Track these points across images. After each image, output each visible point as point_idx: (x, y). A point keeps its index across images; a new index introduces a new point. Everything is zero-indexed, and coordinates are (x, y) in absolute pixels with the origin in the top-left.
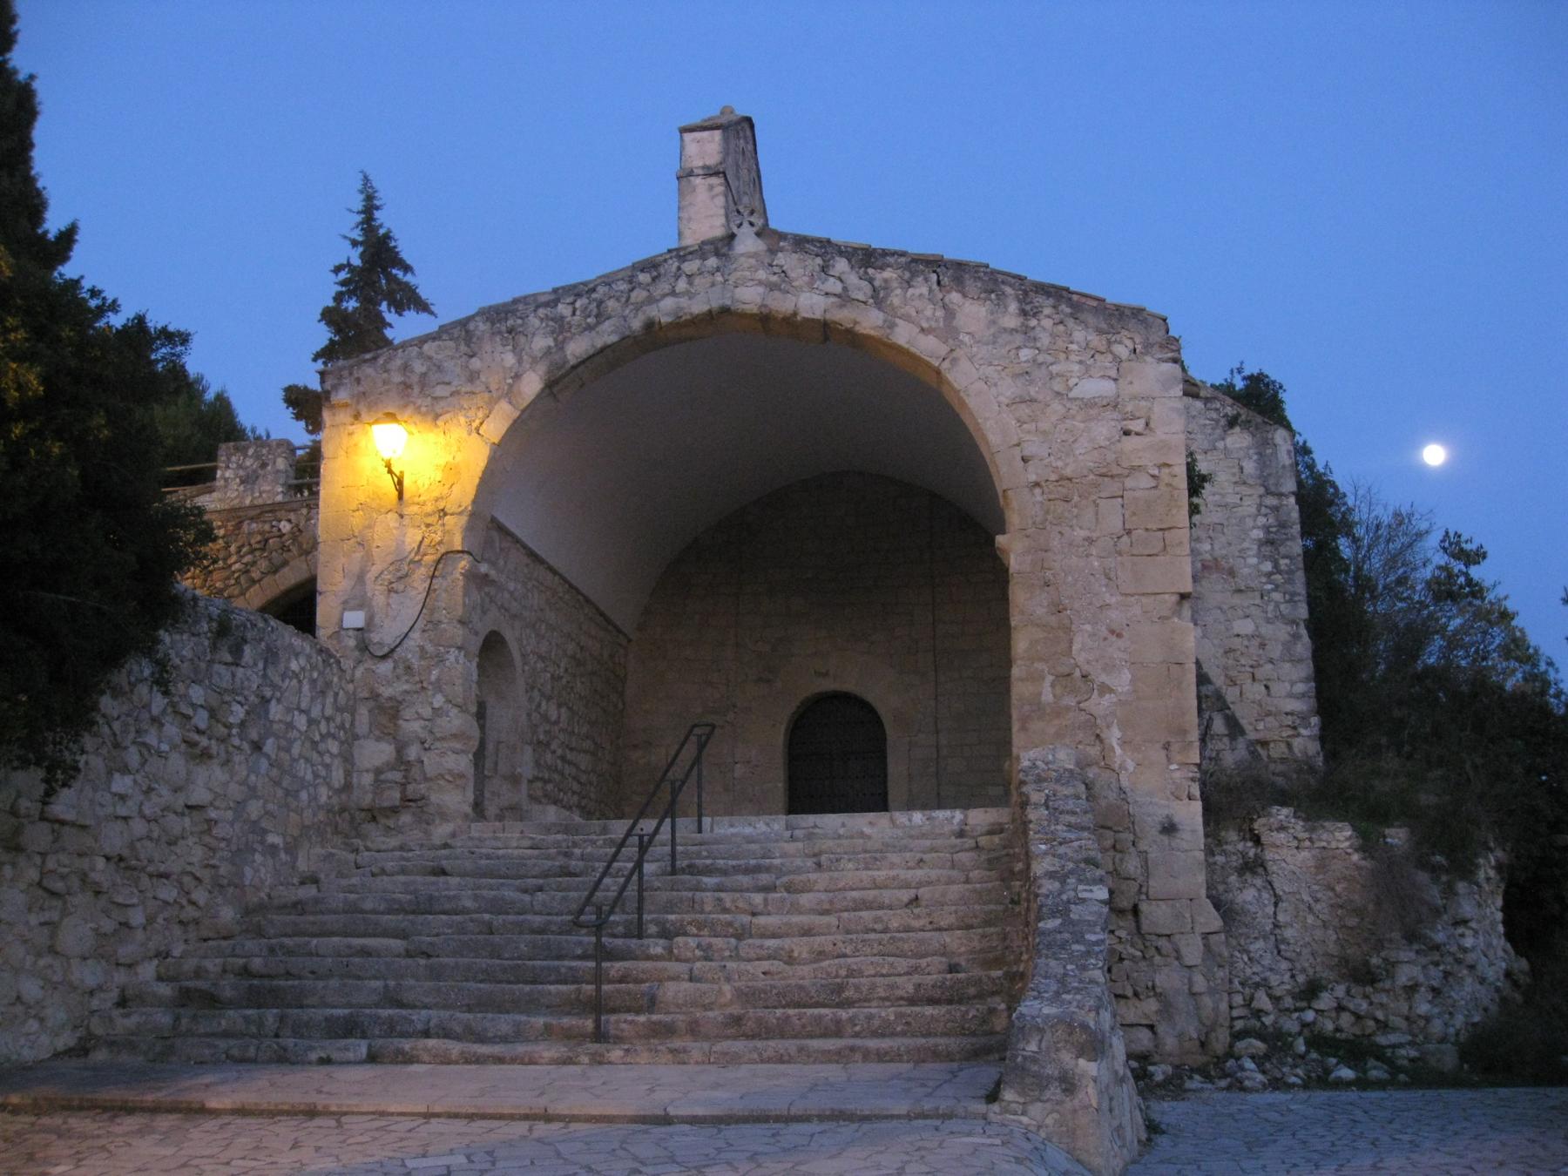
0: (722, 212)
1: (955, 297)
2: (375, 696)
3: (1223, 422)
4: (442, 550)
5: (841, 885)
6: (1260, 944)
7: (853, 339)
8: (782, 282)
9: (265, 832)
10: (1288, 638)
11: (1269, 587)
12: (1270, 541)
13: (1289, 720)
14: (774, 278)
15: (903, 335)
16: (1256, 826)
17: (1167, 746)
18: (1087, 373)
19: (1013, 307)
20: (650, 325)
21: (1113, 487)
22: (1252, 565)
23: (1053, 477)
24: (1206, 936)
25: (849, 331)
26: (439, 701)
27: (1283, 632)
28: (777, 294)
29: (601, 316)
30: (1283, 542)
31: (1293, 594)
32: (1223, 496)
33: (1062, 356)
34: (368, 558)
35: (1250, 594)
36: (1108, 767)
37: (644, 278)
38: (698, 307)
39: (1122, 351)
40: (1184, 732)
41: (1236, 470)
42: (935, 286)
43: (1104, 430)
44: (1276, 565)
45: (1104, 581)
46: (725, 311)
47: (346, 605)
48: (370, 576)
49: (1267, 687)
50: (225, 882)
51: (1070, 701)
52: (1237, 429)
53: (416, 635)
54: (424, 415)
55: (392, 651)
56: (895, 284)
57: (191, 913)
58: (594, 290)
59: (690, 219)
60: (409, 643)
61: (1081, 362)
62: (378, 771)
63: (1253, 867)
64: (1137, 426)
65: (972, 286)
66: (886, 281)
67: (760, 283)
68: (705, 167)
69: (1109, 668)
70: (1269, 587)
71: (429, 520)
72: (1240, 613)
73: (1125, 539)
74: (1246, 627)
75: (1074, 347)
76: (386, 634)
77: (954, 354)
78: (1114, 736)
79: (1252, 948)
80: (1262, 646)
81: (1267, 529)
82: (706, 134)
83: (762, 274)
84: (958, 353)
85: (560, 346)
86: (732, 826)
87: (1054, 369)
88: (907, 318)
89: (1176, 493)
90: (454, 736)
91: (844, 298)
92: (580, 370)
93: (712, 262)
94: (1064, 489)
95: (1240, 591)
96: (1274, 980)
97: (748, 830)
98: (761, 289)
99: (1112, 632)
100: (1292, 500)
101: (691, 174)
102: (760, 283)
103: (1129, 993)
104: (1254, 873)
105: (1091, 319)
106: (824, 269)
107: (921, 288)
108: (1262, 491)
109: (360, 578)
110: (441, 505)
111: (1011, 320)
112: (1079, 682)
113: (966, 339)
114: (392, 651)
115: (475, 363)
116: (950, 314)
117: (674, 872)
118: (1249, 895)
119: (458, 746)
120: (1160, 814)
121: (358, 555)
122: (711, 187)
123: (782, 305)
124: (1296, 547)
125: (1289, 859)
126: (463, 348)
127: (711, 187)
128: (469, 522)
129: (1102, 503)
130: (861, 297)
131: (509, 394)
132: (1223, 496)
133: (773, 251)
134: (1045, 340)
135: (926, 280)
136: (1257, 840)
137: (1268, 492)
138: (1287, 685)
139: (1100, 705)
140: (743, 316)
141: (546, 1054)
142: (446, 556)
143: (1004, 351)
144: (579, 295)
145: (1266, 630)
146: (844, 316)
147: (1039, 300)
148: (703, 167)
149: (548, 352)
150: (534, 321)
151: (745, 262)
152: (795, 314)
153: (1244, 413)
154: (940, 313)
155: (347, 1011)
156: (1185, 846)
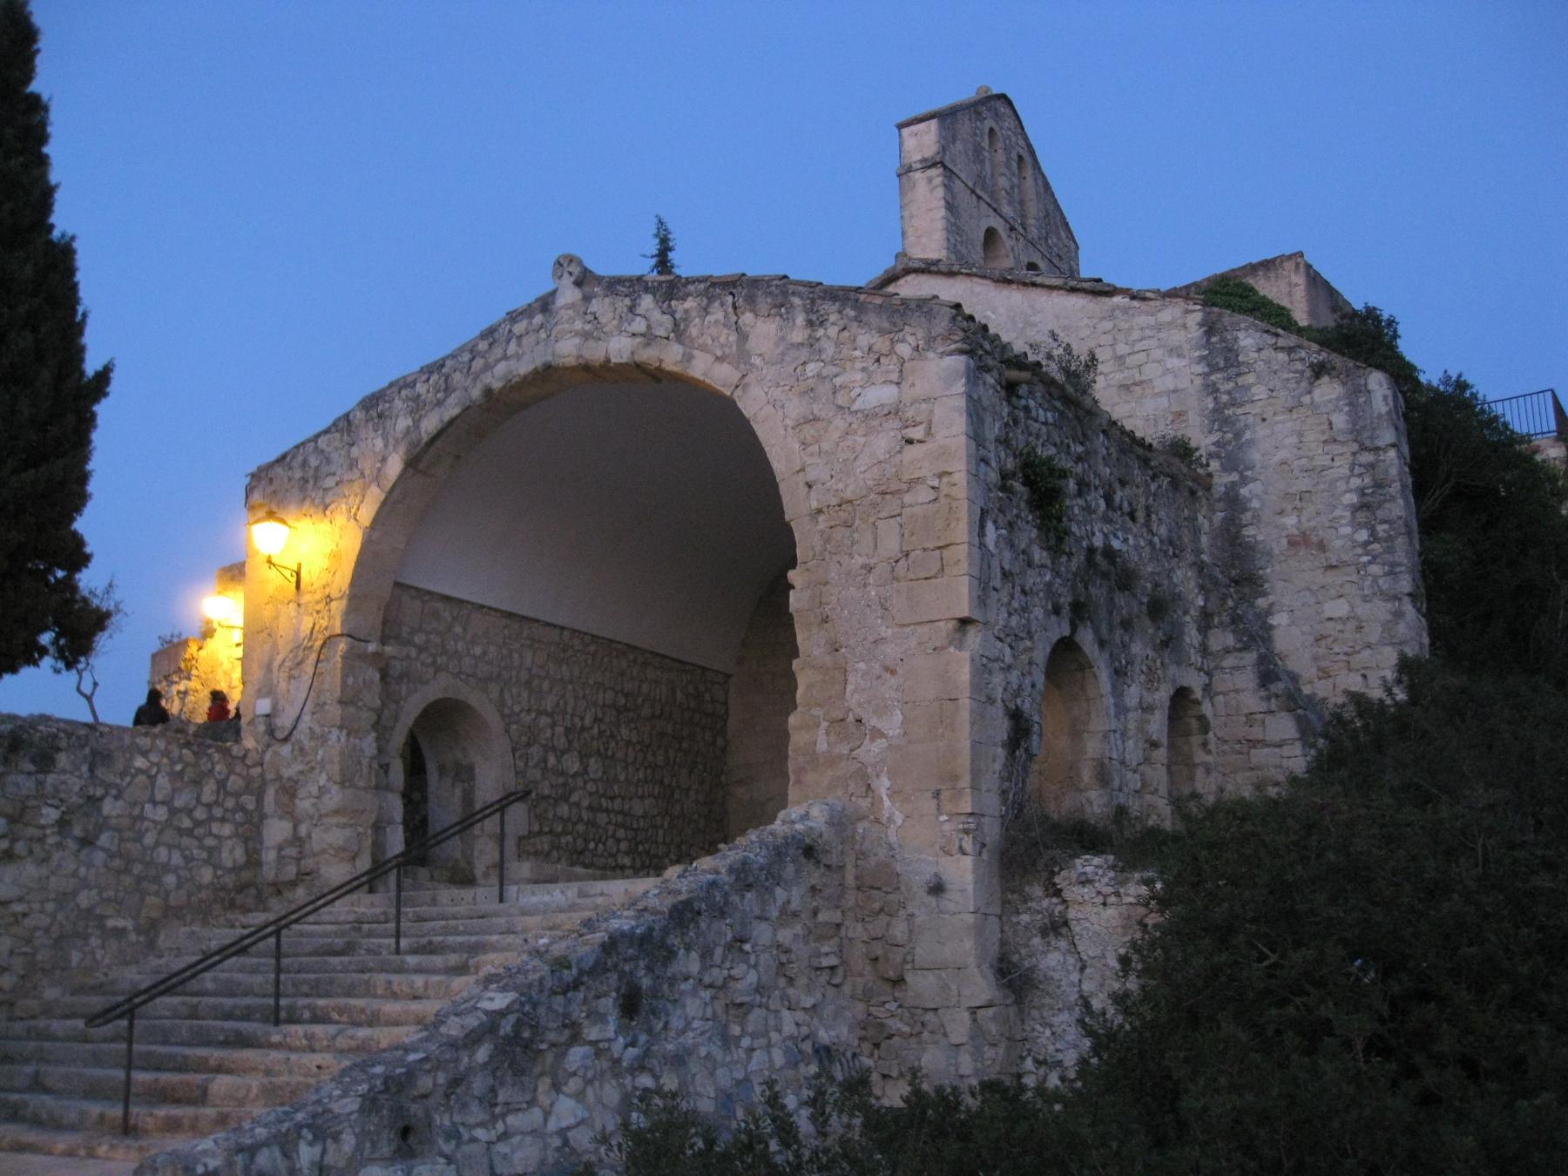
0: (942, 203)
1: (747, 317)
2: (279, 778)
3: (1308, 373)
4: (327, 634)
6: (1065, 1016)
7: (656, 375)
9: (102, 918)
10: (1389, 617)
11: (1365, 559)
12: (1365, 506)
14: (588, 327)
15: (702, 368)
16: (1057, 880)
17: (937, 794)
18: (869, 381)
19: (800, 319)
21: (891, 505)
22: (1345, 535)
23: (834, 502)
24: (973, 1011)
27: (1380, 610)
28: (591, 343)
29: (448, 390)
30: (1380, 505)
31: (1394, 565)
32: (1311, 459)
34: (275, 649)
35: (1347, 569)
36: (877, 821)
38: (524, 368)
39: (904, 350)
40: (955, 778)
41: (1325, 427)
42: (730, 309)
43: (883, 442)
45: (880, 612)
48: (276, 664)
49: (1364, 676)
51: (844, 749)
52: (1325, 379)
53: (306, 718)
54: (317, 507)
55: (290, 734)
58: (443, 366)
59: (912, 217)
60: (303, 726)
61: (863, 369)
62: (280, 848)
63: (1057, 927)
64: (917, 433)
65: (764, 303)
66: (686, 311)
67: (577, 334)
68: (924, 160)
69: (882, 710)
70: (1365, 559)
71: (318, 607)
73: (902, 562)
74: (1339, 608)
75: (858, 353)
76: (284, 721)
77: (746, 380)
78: (883, 784)
79: (1056, 1020)
80: (1359, 628)
81: (1361, 492)
83: (578, 325)
84: (751, 378)
85: (417, 424)
86: (534, 894)
87: (838, 381)
88: (704, 348)
89: (954, 505)
90: (336, 812)
91: (649, 337)
92: (438, 444)
93: (538, 319)
95: (1332, 567)
97: (547, 898)
98: (577, 340)
99: (887, 669)
101: (910, 170)
102: (577, 334)
104: (1058, 934)
105: (873, 319)
106: (631, 309)
107: (717, 314)
108: (1355, 447)
109: (269, 668)
110: (327, 591)
111: (798, 335)
112: (851, 727)
114: (290, 734)
115: (355, 451)
116: (743, 337)
118: (1053, 959)
119: (342, 820)
120: (927, 873)
121: (267, 647)
122: (930, 180)
123: (595, 353)
125: (1093, 919)
128: (349, 606)
129: (880, 524)
130: (663, 334)
131: (378, 478)
132: (1311, 459)
133: (587, 299)
134: (829, 350)
135: (722, 305)
136: (1058, 893)
137: (1363, 448)
139: (872, 750)
140: (566, 369)
142: (329, 641)
143: (791, 370)
144: (431, 373)
145: (1363, 610)
146: (648, 355)
147: (830, 309)
148: (921, 161)
149: (408, 431)
150: (398, 404)
151: (566, 314)
153: (1337, 360)
154: (733, 338)
156: (951, 907)
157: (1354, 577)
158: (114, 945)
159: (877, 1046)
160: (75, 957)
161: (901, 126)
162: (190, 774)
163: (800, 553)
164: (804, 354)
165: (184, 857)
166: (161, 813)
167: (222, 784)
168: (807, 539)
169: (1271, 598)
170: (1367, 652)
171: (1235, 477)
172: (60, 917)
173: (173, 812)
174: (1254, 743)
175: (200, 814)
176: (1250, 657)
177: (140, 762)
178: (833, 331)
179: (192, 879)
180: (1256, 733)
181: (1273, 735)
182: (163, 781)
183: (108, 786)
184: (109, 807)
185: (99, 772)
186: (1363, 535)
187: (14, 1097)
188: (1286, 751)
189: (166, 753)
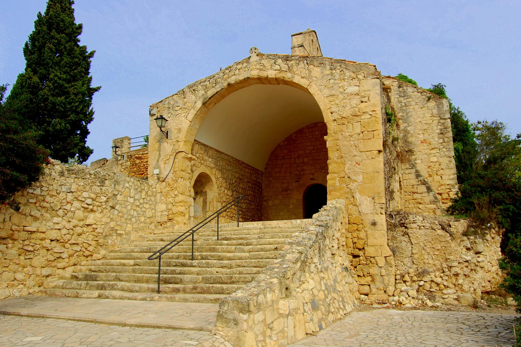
5: (260, 243)
6: (407, 259)
8: (263, 68)
11: (442, 147)
13: (448, 187)
15: (297, 80)
20: (229, 85)
21: (358, 119)
22: (436, 140)
23: (340, 117)
25: (283, 80)
26: (176, 193)
28: (262, 71)
33: (343, 81)
36: (355, 205)
37: (227, 71)
38: (241, 78)
39: (361, 77)
42: (306, 64)
43: (355, 101)
44: (444, 140)
46: (248, 78)
47: (155, 168)
50: (102, 244)
53: (171, 175)
56: (294, 65)
57: (87, 253)
62: (162, 212)
67: (258, 69)
70: (442, 147)
72: (433, 155)
73: (361, 135)
74: (435, 159)
76: (163, 176)
80: (440, 165)
82: (298, 36)
83: (258, 67)
85: (206, 92)
87: (340, 85)
88: (298, 74)
91: (280, 70)
92: (212, 99)
93: (245, 64)
94: (343, 120)
96: (411, 270)
98: (258, 71)
100: (449, 120)
102: (258, 69)
103: (362, 275)
105: (351, 69)
107: (302, 65)
108: (439, 118)
113: (315, 79)
116: (310, 72)
117: (218, 240)
122: (300, 50)
123: (264, 74)
124: (450, 134)
126: (183, 96)
127: (300, 50)
138: (448, 176)
141: (139, 297)
149: (203, 95)
152: (267, 77)
154: (307, 72)
155: (102, 282)
157: (438, 151)
158: (119, 238)
159: (356, 267)
160: (110, 241)
161: (292, 36)
162: (139, 190)
163: (329, 131)
164: (330, 77)
165: (138, 214)
166: (132, 200)
167: (147, 193)
168: (331, 127)
169: (416, 156)
170: (442, 171)
171: (406, 125)
172: (105, 230)
173: (135, 200)
174: (414, 193)
175: (141, 201)
176: (413, 171)
177: (127, 185)
178: (338, 71)
179: (139, 220)
180: (415, 190)
181: (419, 191)
182: (132, 191)
183: (118, 191)
184: (119, 197)
185: (117, 187)
186: (441, 141)
187: (111, 283)
188: (423, 195)
189: (133, 183)
